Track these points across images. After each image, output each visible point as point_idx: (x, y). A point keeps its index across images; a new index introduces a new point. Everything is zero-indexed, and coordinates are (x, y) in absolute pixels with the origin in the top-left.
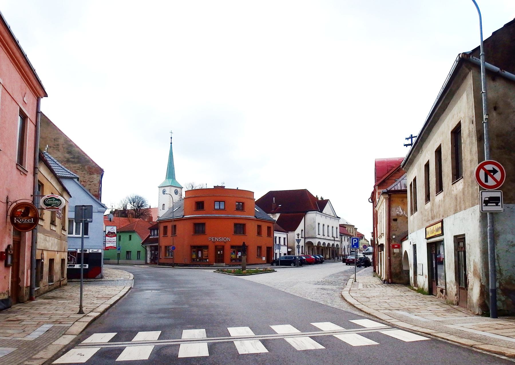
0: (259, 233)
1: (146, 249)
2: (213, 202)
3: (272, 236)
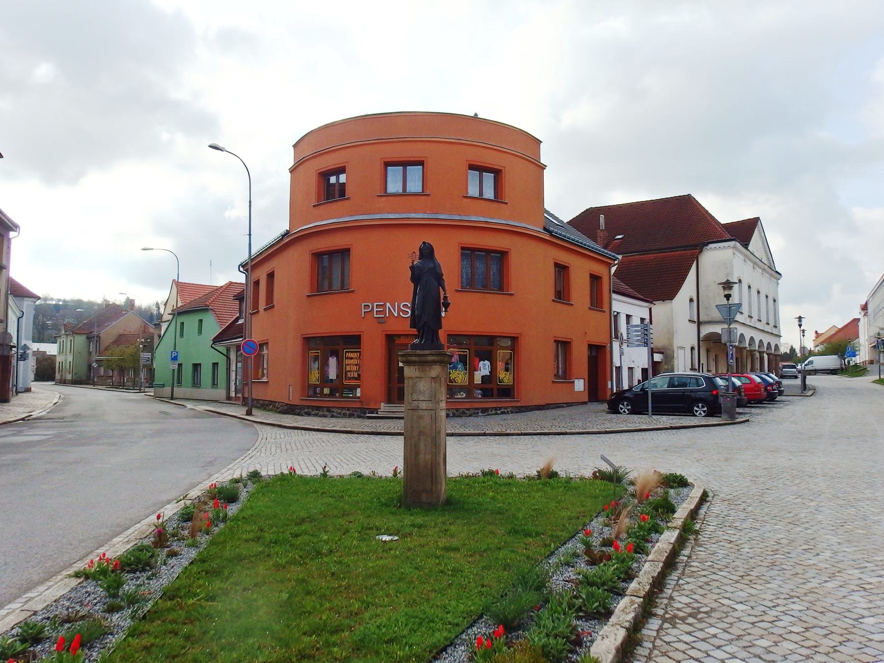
0: (562, 294)
1: (228, 358)
2: (379, 166)
3: (606, 308)
